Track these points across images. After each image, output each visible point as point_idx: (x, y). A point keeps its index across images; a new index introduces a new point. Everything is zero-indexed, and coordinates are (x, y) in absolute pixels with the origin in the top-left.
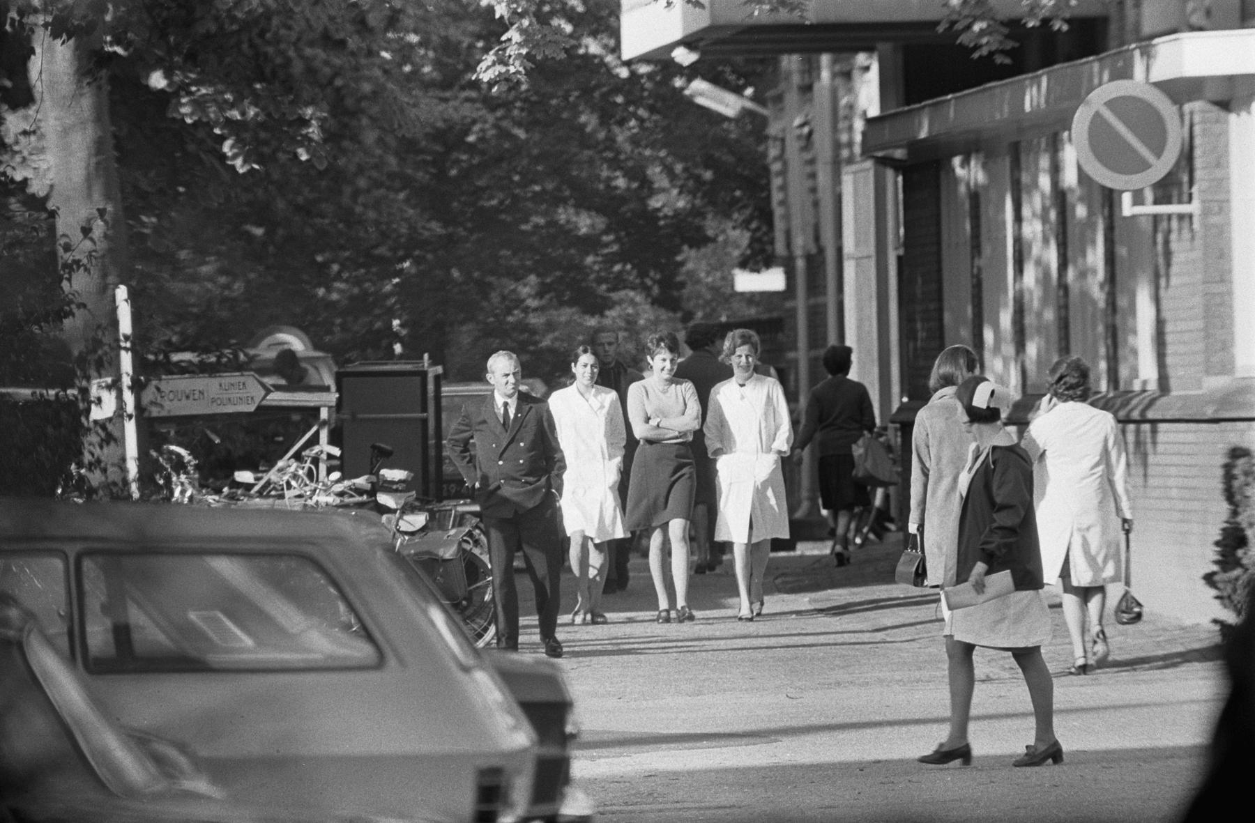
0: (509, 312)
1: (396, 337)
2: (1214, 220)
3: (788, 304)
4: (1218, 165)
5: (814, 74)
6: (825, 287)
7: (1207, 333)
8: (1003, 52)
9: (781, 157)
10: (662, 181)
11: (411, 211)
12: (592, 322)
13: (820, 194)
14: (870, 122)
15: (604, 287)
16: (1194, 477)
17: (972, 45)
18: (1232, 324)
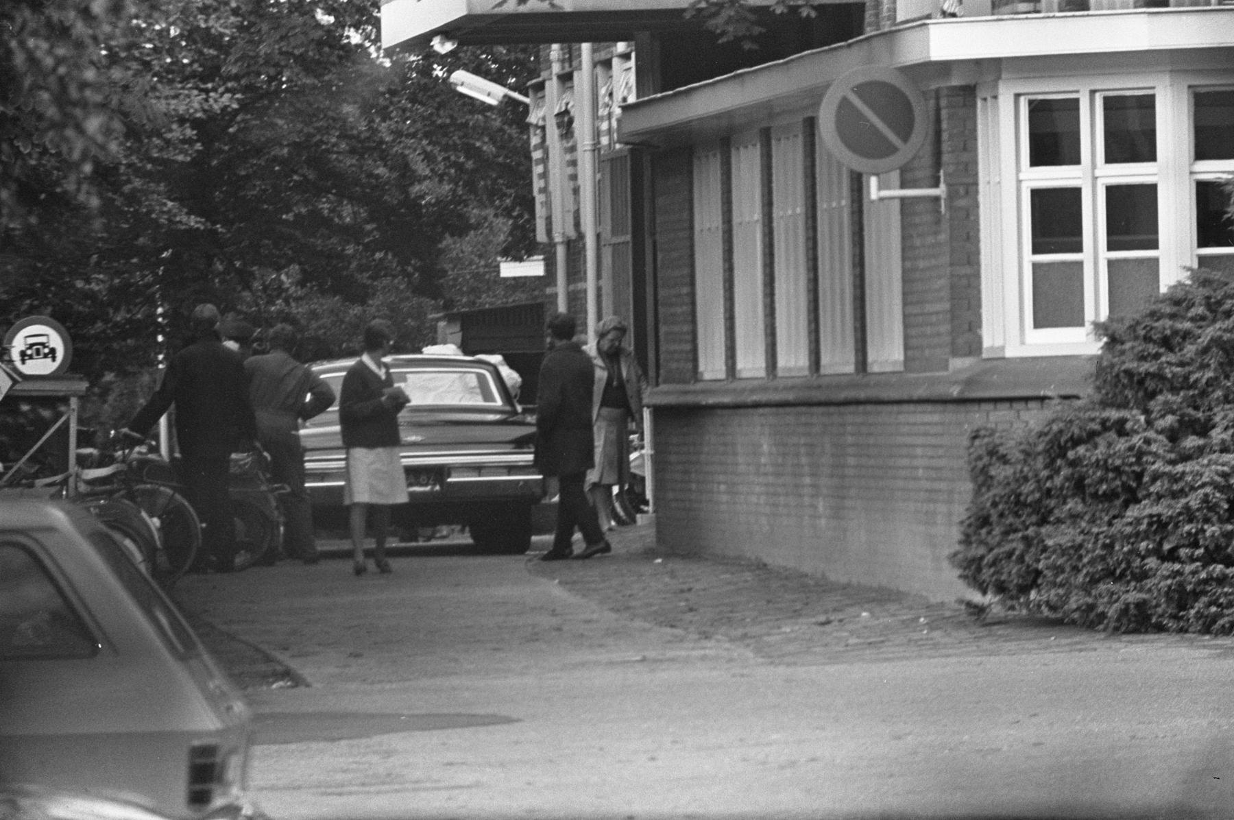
0: (271, 302)
1: (160, 329)
2: (962, 203)
3: (548, 291)
4: (965, 149)
5: (575, 63)
6: (585, 273)
7: (953, 315)
8: (753, 39)
9: (542, 144)
10: (421, 168)
11: (170, 204)
12: (356, 310)
13: (580, 182)
14: (626, 108)
15: (366, 275)
16: (940, 457)
17: (718, 31)
18: (979, 306)
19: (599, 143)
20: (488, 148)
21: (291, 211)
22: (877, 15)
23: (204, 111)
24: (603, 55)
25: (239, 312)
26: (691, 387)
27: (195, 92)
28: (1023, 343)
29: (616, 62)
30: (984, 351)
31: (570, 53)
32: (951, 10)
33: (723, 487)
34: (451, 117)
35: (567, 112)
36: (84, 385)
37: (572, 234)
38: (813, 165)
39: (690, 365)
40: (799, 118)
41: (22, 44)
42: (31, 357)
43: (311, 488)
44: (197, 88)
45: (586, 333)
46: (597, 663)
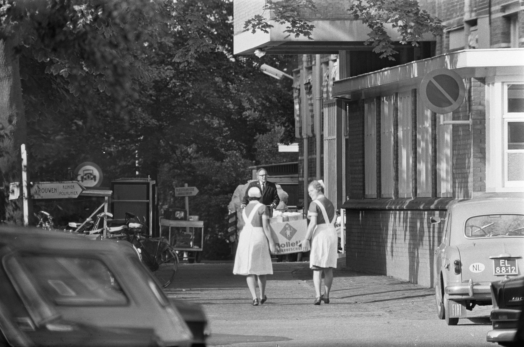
5: (313, 63)
6: (316, 151)
10: (246, 105)
13: (314, 113)
14: (335, 83)
19: (322, 96)
21: (193, 121)
22: (441, 46)
24: (325, 60)
26: (362, 201)
31: (311, 58)
32: (473, 46)
33: (375, 244)
35: (309, 83)
37: (311, 135)
38: (415, 109)
39: (362, 192)
40: (411, 89)
42: (86, 179)
43: (123, 218)
44: (156, 67)
46: (323, 316)
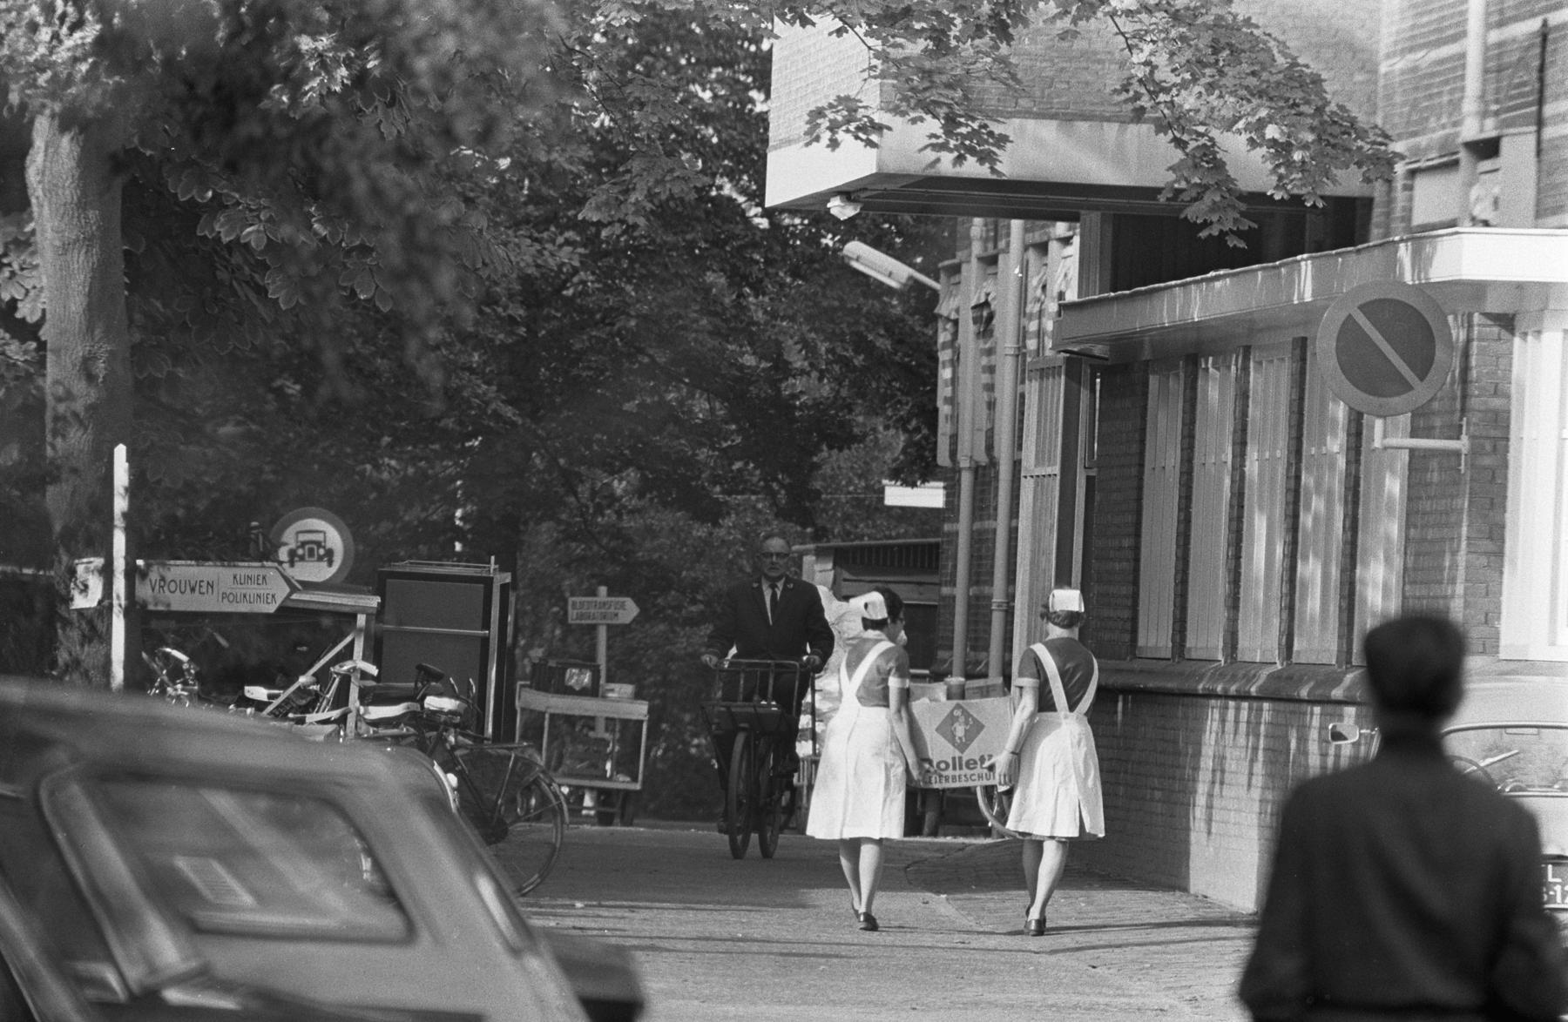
3: (947, 527)
5: (1002, 244)
6: (996, 509)
8: (1239, 234)
9: (952, 343)
13: (997, 394)
14: (1065, 308)
20: (884, 344)
22: (1388, 214)
23: (538, 266)
24: (1037, 237)
25: (559, 522)
26: (1124, 665)
27: (529, 241)
28: (1553, 644)
29: (1054, 246)
30: (1501, 649)
31: (996, 230)
32: (1483, 216)
34: (841, 300)
35: (986, 304)
36: (374, 601)
37: (983, 459)
38: (1301, 398)
39: (1127, 637)
41: (365, 170)
42: (302, 558)
44: (530, 237)
45: (992, 585)
